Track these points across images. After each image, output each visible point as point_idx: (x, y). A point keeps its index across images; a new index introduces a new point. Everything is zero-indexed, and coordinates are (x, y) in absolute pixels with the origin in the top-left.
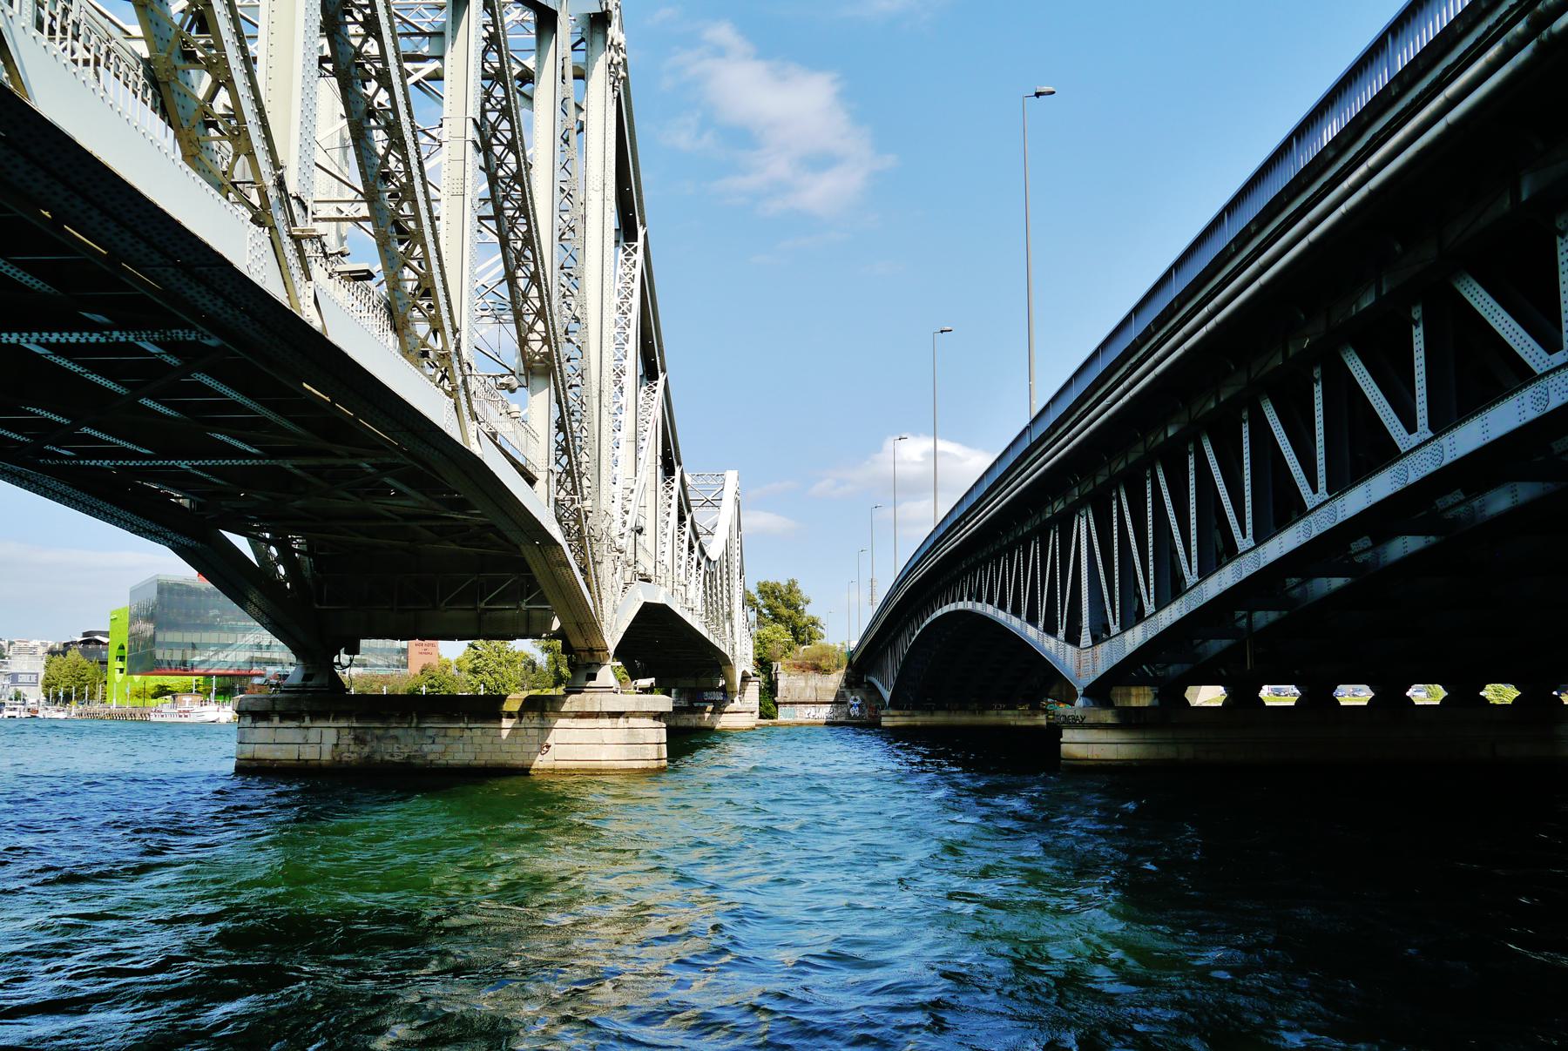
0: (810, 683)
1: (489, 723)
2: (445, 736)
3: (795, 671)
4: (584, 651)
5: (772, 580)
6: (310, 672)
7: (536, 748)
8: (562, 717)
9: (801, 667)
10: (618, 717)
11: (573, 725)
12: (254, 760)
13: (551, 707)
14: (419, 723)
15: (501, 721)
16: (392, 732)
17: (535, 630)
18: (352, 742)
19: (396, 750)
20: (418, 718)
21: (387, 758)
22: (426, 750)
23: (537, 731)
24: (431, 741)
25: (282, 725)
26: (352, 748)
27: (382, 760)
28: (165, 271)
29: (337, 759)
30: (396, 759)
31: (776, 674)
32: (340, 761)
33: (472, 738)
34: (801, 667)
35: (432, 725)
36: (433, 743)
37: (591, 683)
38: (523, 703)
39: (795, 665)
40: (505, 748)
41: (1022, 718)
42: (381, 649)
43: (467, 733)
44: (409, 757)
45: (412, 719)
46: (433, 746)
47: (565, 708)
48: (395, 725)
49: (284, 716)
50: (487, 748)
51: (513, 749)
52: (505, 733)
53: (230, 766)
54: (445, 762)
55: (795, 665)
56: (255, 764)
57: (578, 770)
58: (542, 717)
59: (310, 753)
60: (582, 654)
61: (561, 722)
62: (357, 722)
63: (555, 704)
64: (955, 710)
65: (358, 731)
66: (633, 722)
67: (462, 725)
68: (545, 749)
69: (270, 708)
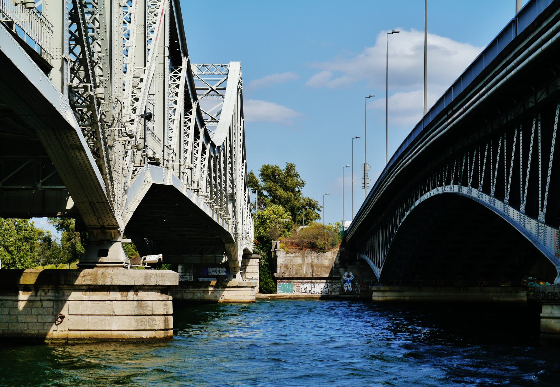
0: (306, 261)
7: (50, 319)
9: (298, 245)
11: (85, 298)
15: (17, 294)
31: (275, 252)
37: (104, 259)
39: (292, 244)
51: (29, 320)
52: (21, 305)
55: (292, 244)
61: (74, 295)
66: (142, 295)
68: (59, 320)
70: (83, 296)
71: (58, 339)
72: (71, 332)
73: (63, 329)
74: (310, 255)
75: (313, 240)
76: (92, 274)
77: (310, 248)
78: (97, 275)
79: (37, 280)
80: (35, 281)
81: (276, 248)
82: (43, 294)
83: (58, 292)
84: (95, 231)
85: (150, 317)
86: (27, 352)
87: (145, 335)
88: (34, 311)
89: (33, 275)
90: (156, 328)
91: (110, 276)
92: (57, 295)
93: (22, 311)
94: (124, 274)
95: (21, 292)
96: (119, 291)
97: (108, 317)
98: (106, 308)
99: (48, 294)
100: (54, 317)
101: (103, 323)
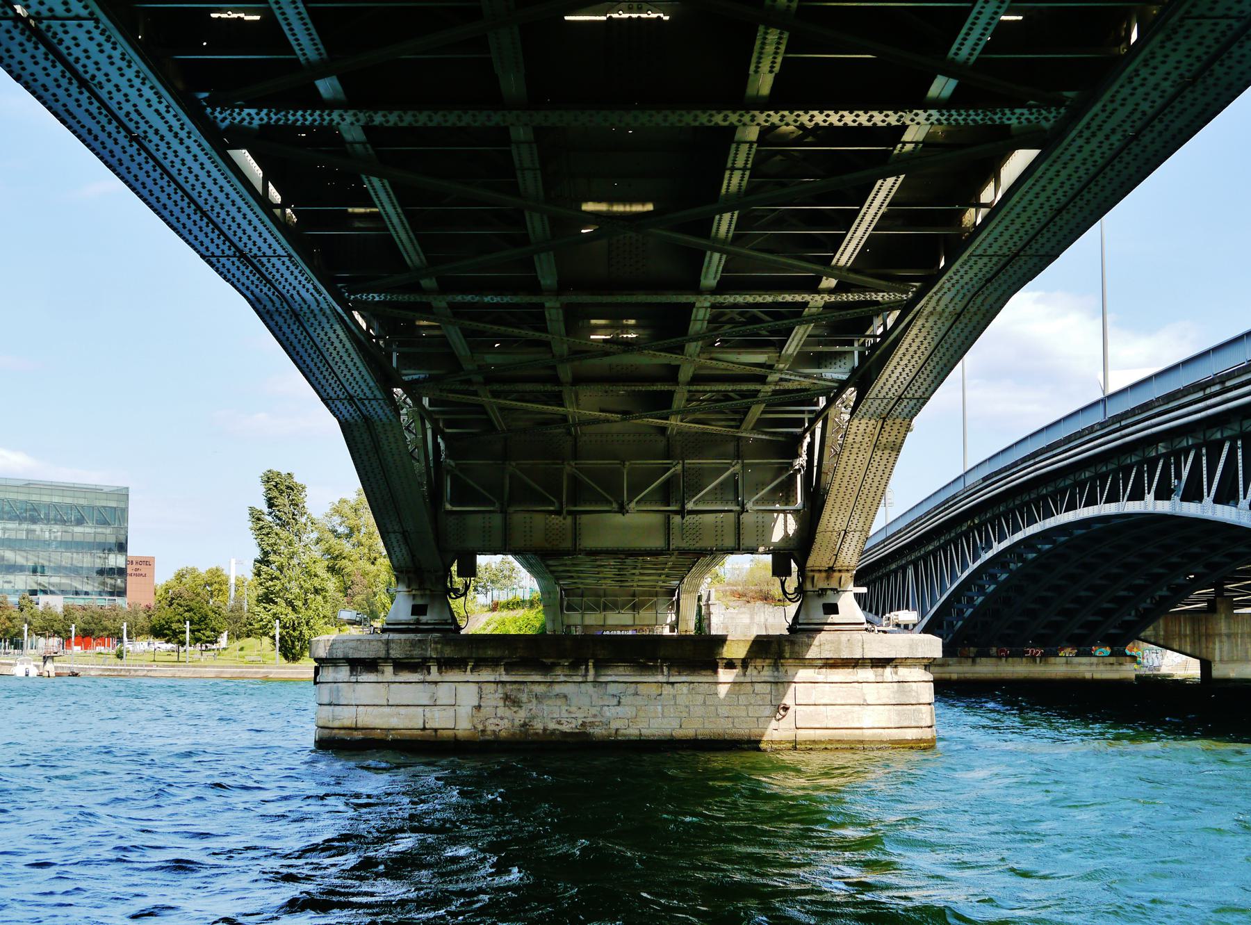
0: (757, 619)
1: (700, 675)
2: (636, 694)
3: (733, 602)
4: (820, 571)
5: (275, 469)
6: (419, 602)
7: (768, 711)
8: (805, 666)
9: (741, 595)
10: (884, 667)
11: (820, 678)
12: (356, 729)
13: (792, 653)
14: (597, 675)
15: (716, 672)
16: (558, 689)
17: (747, 541)
18: (501, 703)
19: (564, 714)
20: (596, 667)
21: (552, 726)
22: (608, 714)
23: (768, 686)
24: (615, 701)
25: (398, 679)
26: (500, 712)
27: (545, 730)
28: (1199, 24)
29: (480, 727)
30: (566, 728)
31: (708, 606)
32: (483, 731)
33: (675, 697)
34: (741, 595)
35: (618, 676)
36: (619, 703)
37: (833, 618)
38: (751, 647)
39: (733, 593)
40: (723, 711)
41: (1102, 667)
42: (88, 569)
43: (667, 690)
44: (583, 724)
45: (587, 670)
46: (619, 709)
47: (812, 653)
48: (562, 678)
49: (400, 665)
50: (698, 711)
51: (735, 713)
52: (723, 690)
53: (310, 742)
54: (637, 732)
55: (733, 593)
56: (358, 735)
57: (830, 742)
58: (776, 666)
59: (440, 720)
60: (817, 575)
61: (803, 674)
62: (507, 674)
63: (797, 648)
64: (1007, 656)
65: (508, 687)
66: (904, 673)
67: (660, 678)
68: (781, 711)
69: (382, 654)
70: (816, 675)
71: (780, 742)
72: (800, 731)
73: (787, 726)
74: (762, 610)
75: (765, 588)
76: (832, 642)
77: (761, 600)
78: (839, 642)
79: (749, 652)
80: (745, 653)
81: (709, 599)
82: (755, 672)
83: (777, 670)
84: (817, 575)
85: (914, 707)
86: (735, 760)
87: (910, 734)
88: (743, 700)
89: (741, 644)
90: (923, 724)
91: (860, 644)
92: (776, 674)
93: (724, 699)
94: (881, 641)
95: (720, 671)
96: (872, 667)
97: (857, 708)
98: (852, 693)
99: (762, 673)
100: (772, 708)
101: (850, 717)
